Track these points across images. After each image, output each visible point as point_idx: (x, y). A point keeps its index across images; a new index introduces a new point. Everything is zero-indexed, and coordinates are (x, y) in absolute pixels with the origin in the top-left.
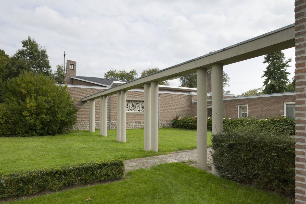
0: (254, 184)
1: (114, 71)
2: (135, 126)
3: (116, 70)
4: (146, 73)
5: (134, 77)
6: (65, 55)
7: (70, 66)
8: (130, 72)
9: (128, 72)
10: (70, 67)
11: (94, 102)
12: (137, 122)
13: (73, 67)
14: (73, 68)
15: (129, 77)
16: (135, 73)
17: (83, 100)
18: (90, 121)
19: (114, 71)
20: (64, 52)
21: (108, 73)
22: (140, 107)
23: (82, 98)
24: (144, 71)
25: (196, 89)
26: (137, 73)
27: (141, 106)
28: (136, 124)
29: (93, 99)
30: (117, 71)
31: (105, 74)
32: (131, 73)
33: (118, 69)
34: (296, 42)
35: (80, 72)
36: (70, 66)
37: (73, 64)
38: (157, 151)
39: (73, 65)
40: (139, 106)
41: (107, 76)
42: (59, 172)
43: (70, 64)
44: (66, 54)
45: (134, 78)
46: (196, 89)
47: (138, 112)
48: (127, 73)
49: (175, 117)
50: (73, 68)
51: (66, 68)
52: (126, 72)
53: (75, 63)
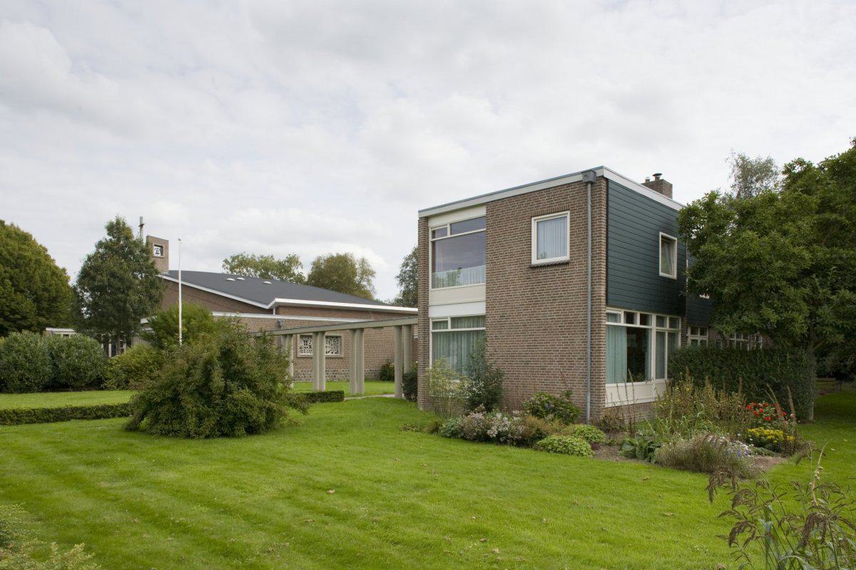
0: (806, 323)
4: (321, 261)
6: (141, 226)
10: (155, 252)
14: (159, 255)
16: (297, 262)
20: (141, 218)
21: (234, 259)
24: (319, 259)
25: (415, 310)
27: (328, 345)
31: (226, 261)
32: (288, 261)
33: (255, 249)
39: (162, 247)
42: (644, 415)
43: (156, 246)
45: (294, 274)
46: (415, 310)
49: (384, 363)
50: (159, 255)
52: (276, 260)
53: (167, 241)
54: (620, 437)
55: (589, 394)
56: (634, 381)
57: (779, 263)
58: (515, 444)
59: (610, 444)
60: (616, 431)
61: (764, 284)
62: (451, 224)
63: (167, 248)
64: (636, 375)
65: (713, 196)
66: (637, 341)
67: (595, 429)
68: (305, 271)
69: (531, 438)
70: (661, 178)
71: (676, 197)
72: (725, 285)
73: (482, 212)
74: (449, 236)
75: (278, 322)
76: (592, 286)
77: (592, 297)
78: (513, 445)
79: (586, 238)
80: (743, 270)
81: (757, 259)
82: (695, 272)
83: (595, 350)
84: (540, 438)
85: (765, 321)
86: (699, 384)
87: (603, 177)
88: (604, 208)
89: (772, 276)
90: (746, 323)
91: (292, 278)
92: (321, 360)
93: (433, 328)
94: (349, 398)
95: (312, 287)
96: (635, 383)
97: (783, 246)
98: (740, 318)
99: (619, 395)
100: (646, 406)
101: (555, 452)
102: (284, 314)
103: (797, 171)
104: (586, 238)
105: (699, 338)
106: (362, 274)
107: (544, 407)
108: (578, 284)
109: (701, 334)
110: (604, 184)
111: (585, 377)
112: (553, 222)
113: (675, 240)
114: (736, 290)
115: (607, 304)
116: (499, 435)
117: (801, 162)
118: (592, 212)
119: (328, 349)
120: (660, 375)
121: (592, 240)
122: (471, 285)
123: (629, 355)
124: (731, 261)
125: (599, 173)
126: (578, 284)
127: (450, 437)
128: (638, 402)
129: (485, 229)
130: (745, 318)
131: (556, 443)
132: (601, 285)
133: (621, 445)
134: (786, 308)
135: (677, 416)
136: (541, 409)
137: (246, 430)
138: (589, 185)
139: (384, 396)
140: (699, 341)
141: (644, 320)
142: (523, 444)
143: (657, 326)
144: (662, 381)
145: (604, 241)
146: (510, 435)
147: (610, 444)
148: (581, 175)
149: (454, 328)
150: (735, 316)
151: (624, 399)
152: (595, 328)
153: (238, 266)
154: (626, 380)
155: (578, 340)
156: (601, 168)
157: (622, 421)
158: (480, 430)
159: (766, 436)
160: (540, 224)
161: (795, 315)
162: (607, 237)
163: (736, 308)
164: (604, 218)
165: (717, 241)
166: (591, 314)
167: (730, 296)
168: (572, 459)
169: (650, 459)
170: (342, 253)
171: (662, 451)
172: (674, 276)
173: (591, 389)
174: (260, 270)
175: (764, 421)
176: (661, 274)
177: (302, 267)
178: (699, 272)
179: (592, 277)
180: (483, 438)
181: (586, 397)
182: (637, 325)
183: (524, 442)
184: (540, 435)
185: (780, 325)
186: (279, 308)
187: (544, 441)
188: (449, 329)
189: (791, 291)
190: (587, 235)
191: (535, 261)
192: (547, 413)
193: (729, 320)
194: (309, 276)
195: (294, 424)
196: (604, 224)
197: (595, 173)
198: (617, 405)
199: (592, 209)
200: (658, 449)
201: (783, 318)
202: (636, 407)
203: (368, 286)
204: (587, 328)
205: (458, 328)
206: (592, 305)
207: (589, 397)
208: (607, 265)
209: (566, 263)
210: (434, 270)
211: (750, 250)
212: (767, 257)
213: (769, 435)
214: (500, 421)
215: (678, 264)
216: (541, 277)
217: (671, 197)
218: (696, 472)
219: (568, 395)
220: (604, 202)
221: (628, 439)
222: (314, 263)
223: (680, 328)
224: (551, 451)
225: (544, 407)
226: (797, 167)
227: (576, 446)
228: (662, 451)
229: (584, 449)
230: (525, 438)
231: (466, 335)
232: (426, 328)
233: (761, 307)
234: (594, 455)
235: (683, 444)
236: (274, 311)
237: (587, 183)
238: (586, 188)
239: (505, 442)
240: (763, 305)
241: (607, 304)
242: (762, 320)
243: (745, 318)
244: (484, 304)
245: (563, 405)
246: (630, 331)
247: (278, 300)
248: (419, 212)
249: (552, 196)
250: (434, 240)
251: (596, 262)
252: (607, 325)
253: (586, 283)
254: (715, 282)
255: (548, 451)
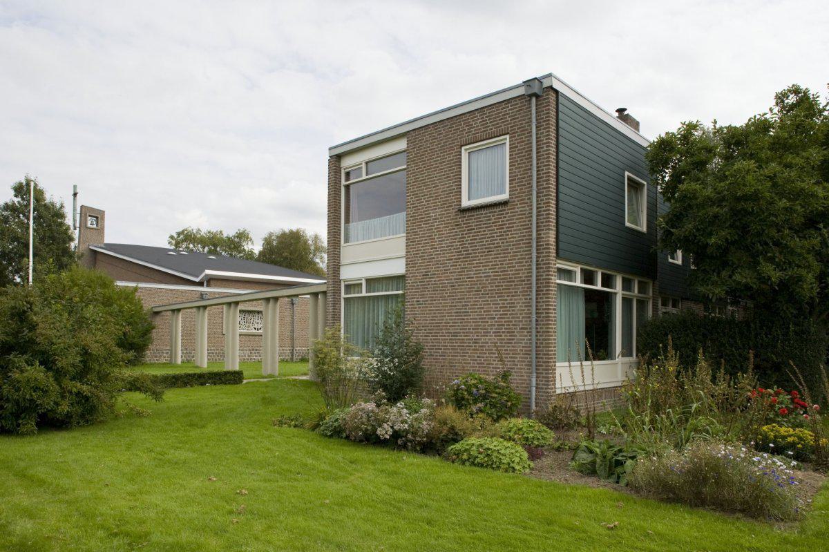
1: (195, 231)
2: (249, 356)
3: (199, 230)
5: (246, 248)
6: (75, 195)
7: (90, 221)
8: (234, 234)
9: (231, 236)
10: (89, 222)
11: (181, 314)
12: (253, 350)
13: (97, 224)
14: (95, 226)
15: (233, 246)
16: (248, 238)
17: (155, 310)
18: (171, 346)
19: (195, 231)
20: (75, 187)
21: (179, 234)
22: (258, 323)
23: (153, 306)
24: (271, 235)
26: (253, 238)
27: (259, 321)
28: (251, 353)
29: (179, 310)
30: (204, 231)
31: (172, 237)
32: (237, 237)
33: (203, 224)
34: (799, 93)
35: (115, 234)
36: (90, 221)
37: (98, 216)
38: (277, 374)
39: (97, 218)
40: (257, 321)
41: (177, 244)
43: (90, 216)
44: (78, 191)
47: (254, 331)
48: (229, 238)
50: (95, 226)
51: (78, 225)
52: (225, 235)
53: (104, 212)
54: (578, 437)
55: (535, 375)
56: (594, 359)
57: (783, 203)
58: (418, 448)
59: (559, 449)
60: (569, 427)
61: (763, 230)
62: (367, 163)
63: (103, 218)
64: (597, 352)
65: (691, 127)
66: (598, 305)
67: (538, 426)
68: (256, 247)
69: (442, 440)
70: (626, 113)
71: (643, 130)
72: (710, 234)
73: (402, 145)
74: (364, 177)
75: (202, 295)
76: (537, 231)
77: (537, 246)
78: (416, 451)
79: (531, 169)
80: (735, 213)
81: (755, 197)
82: (671, 220)
83: (542, 317)
84: (456, 441)
85: (764, 280)
86: (688, 362)
87: (551, 87)
88: (553, 128)
89: (774, 219)
90: (739, 283)
91: (242, 255)
92: (234, 335)
93: (346, 293)
94: (249, 380)
95: (261, 263)
96: (595, 362)
97: (788, 180)
98: (730, 277)
99: (572, 377)
100: (611, 391)
101: (473, 464)
102: (216, 286)
103: (790, 102)
104: (531, 169)
105: (670, 309)
106: (315, 251)
107: (470, 393)
108: (520, 229)
109: (672, 307)
110: (552, 96)
111: (528, 353)
112: (489, 152)
113: (644, 185)
114: (727, 239)
115: (558, 256)
116: (396, 435)
117: (796, 90)
118: (537, 134)
119: (260, 326)
120: (627, 352)
121: (537, 171)
122: (390, 237)
123: (587, 328)
124: (720, 201)
125: (546, 83)
126: (520, 229)
127: (331, 436)
128: (600, 386)
129: (405, 167)
130: (737, 277)
131: (474, 452)
132: (549, 229)
133: (576, 449)
134: (790, 264)
135: (657, 408)
136: (467, 396)
137: (38, 425)
138: (534, 99)
139: (260, 380)
140: (671, 307)
141: (607, 281)
142: (431, 449)
143: (623, 290)
144: (627, 359)
145: (553, 172)
146: (409, 436)
147: (559, 449)
148: (523, 88)
149: (370, 292)
150: (724, 274)
151: (579, 382)
152: (542, 288)
153: (183, 241)
154: (583, 355)
155: (520, 303)
156: (550, 75)
157: (577, 413)
158: (369, 428)
159: (784, 437)
160: (473, 156)
161: (804, 272)
162: (557, 167)
163: (725, 264)
164: (553, 142)
165: (698, 179)
166: (537, 269)
167: (719, 247)
168: (497, 478)
169: (619, 477)
170: (294, 229)
171: (639, 468)
172: (644, 229)
173: (537, 369)
174: (208, 246)
175: (777, 415)
176: (627, 224)
177: (253, 243)
178: (676, 219)
179: (537, 219)
180: (370, 439)
181: (530, 380)
182: (598, 286)
183: (432, 445)
184: (455, 436)
185: (783, 285)
186: (210, 281)
187: (457, 446)
188: (364, 294)
189: (796, 243)
190: (531, 165)
191: (466, 203)
192: (475, 401)
193: (715, 278)
194: (260, 252)
195: (136, 415)
196: (553, 150)
197: (541, 83)
198: (571, 390)
199: (537, 131)
200: (629, 462)
201: (787, 277)
202: (596, 393)
203: (321, 264)
204: (531, 288)
205: (374, 292)
206: (538, 257)
207: (534, 380)
208: (557, 205)
209: (504, 203)
210: (347, 221)
211: (745, 185)
212: (768, 194)
213: (790, 436)
214: (399, 416)
215: (648, 215)
216: (473, 223)
217: (638, 131)
218: (696, 506)
219: (505, 376)
220: (553, 121)
221: (584, 444)
222: (266, 240)
223: (651, 294)
224: (467, 463)
225: (470, 393)
226: (791, 96)
227: (503, 455)
228: (639, 468)
229: (517, 460)
230: (434, 441)
231: (384, 301)
232: (337, 292)
233: (759, 263)
234: (532, 469)
235: (675, 460)
236: (205, 284)
237: (531, 96)
238: (530, 104)
239: (404, 447)
240: (761, 259)
241: (558, 256)
242: (760, 279)
243: (737, 277)
244: (403, 261)
245: (497, 390)
246: (590, 296)
247: (208, 272)
248: (330, 149)
249: (487, 117)
250: (348, 183)
251: (543, 200)
252: (558, 284)
253: (530, 228)
254: (698, 230)
255: (463, 462)
